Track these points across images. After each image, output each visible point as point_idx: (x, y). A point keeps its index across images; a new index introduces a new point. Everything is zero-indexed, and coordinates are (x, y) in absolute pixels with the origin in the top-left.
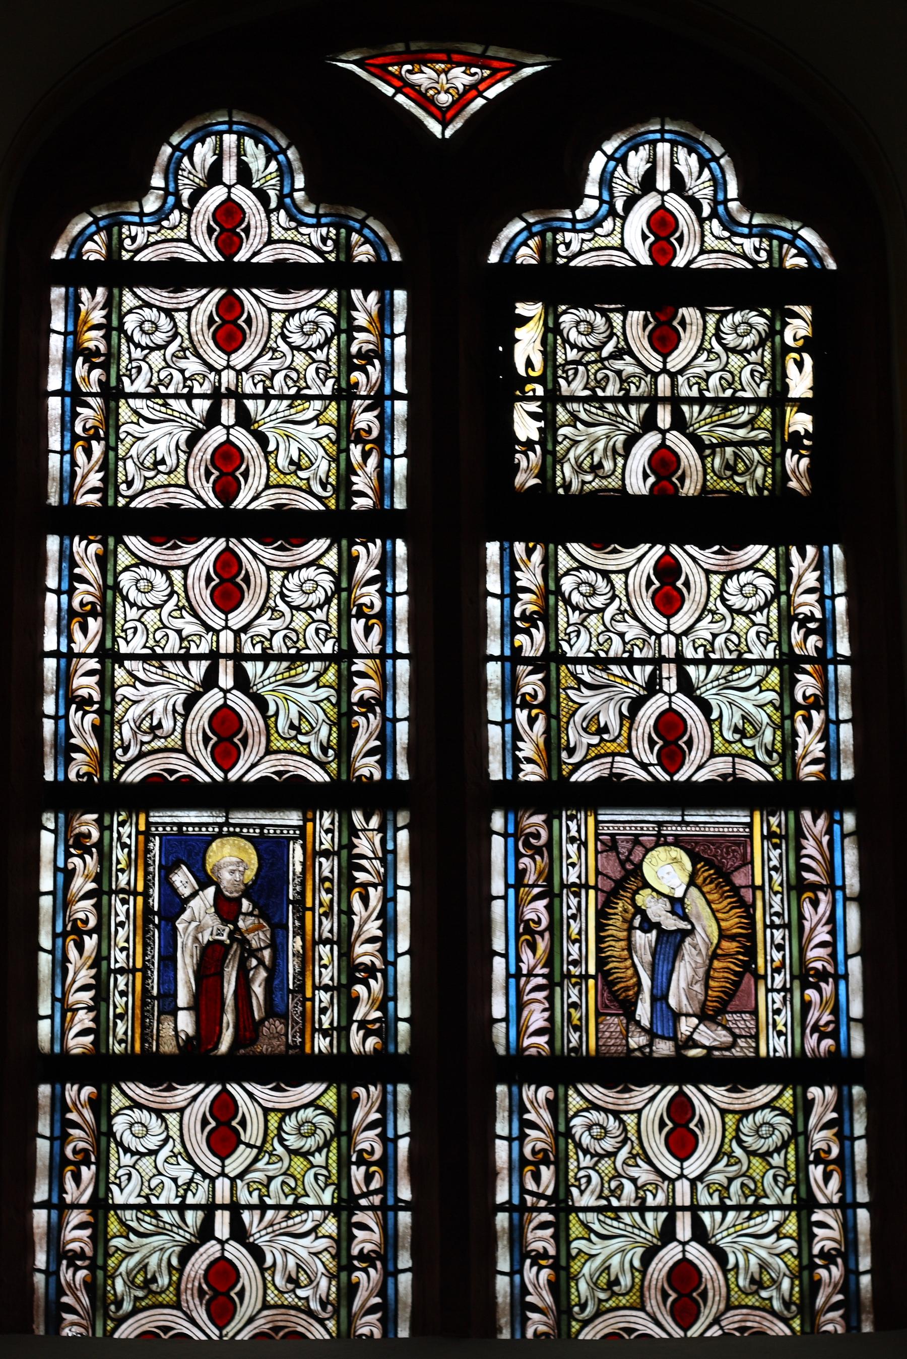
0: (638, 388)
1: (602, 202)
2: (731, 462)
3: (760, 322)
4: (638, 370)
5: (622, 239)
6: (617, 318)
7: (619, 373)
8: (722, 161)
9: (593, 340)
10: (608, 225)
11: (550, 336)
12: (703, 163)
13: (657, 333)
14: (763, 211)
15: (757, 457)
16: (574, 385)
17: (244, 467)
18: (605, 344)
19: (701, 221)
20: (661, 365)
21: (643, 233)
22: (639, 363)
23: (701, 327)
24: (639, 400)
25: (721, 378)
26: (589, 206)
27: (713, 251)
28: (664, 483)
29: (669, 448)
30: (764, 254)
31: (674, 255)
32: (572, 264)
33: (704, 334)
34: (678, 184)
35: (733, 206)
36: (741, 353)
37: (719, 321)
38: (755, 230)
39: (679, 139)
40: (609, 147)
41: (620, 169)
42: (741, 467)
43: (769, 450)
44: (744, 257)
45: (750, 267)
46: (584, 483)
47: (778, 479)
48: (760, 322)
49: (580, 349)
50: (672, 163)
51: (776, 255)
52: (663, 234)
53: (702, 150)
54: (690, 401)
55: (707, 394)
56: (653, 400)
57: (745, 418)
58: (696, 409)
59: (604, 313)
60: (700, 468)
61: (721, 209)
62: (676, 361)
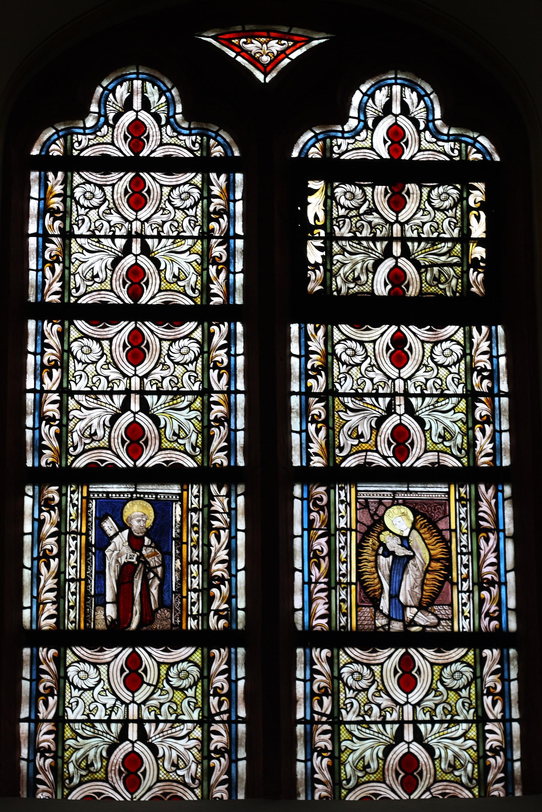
0: (381, 232)
1: (360, 121)
2: (437, 276)
3: (454, 193)
4: (381, 221)
5: (372, 143)
6: (369, 190)
7: (370, 223)
8: (432, 96)
9: (355, 203)
10: (363, 134)
11: (329, 201)
12: (420, 98)
13: (393, 199)
14: (456, 126)
15: (452, 273)
16: (343, 230)
18: (361, 205)
19: (419, 132)
20: (395, 218)
21: (384, 139)
22: (382, 217)
23: (419, 196)
24: (382, 239)
25: (431, 226)
26: (352, 123)
27: (426, 150)
28: (397, 289)
29: (400, 268)
30: (456, 152)
31: (403, 153)
32: (342, 158)
33: (421, 200)
34: (405, 110)
35: (438, 123)
36: (443, 211)
37: (430, 192)
38: (451, 138)
39: (406, 83)
40: (364, 88)
41: (370, 101)
42: (443, 279)
43: (460, 269)
44: (445, 153)
45: (448, 159)
46: (349, 288)
47: (465, 286)
48: (454, 193)
49: (346, 209)
50: (402, 97)
51: (464, 153)
52: (396, 140)
53: (420, 90)
54: (412, 240)
55: (423, 235)
56: (390, 239)
57: (445, 250)
58: (416, 244)
59: (361, 187)
60: (418, 279)
61: (431, 125)
62: (404, 216)
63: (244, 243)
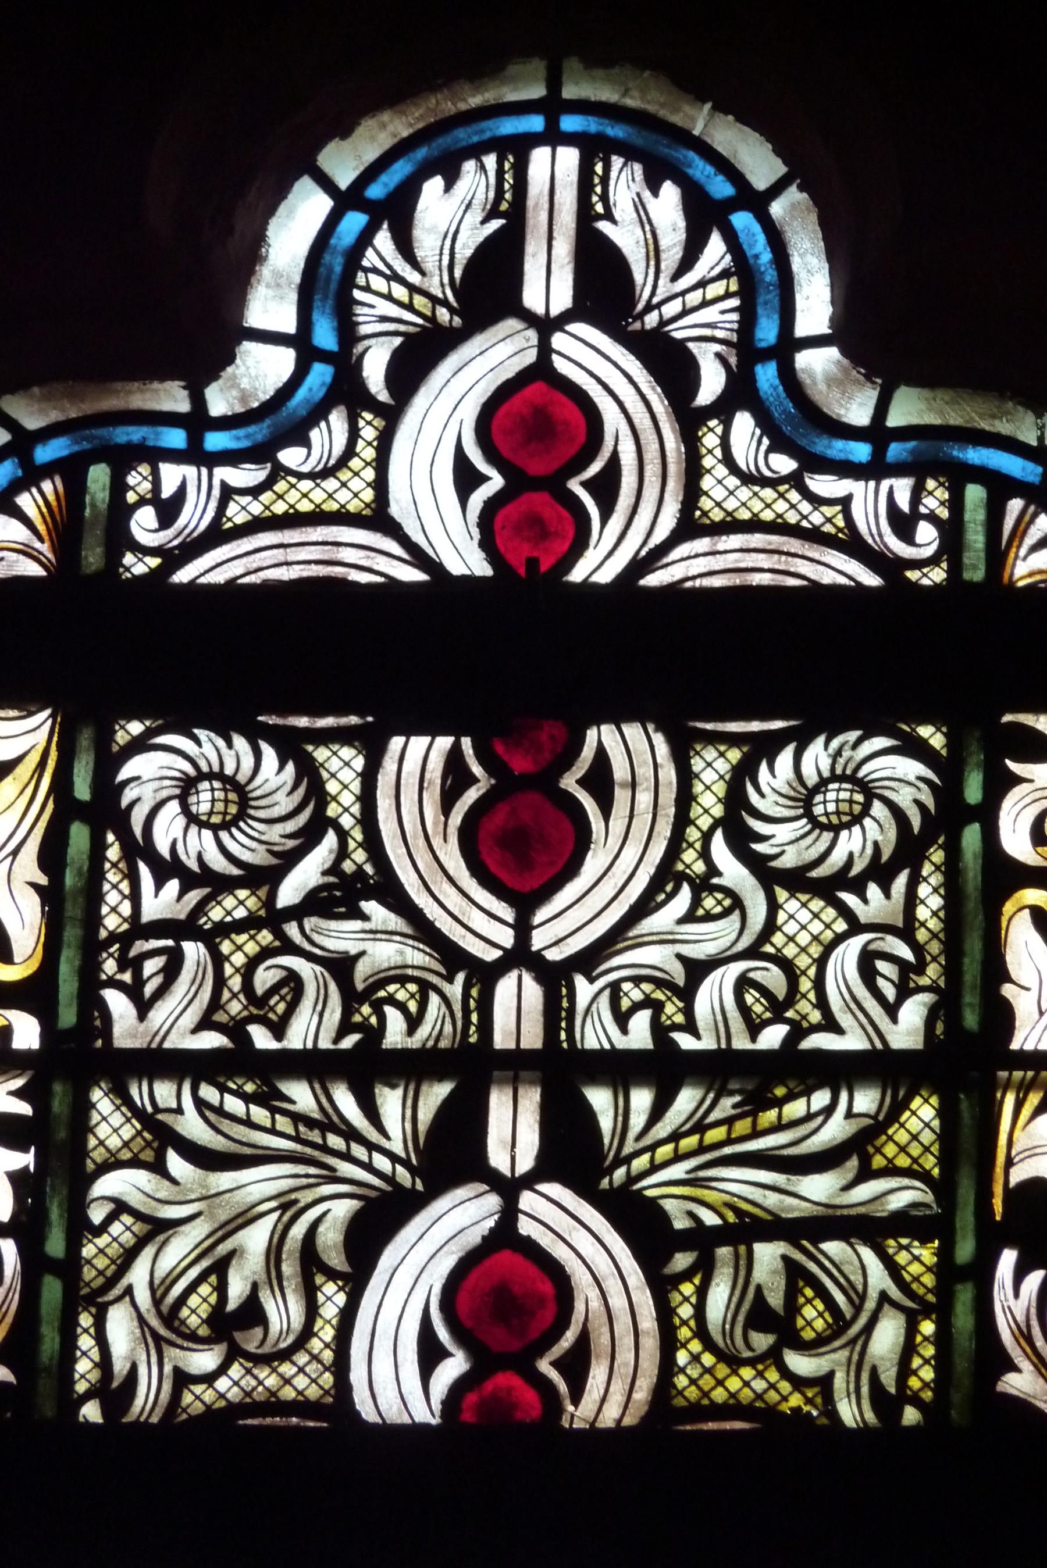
0: (413, 1023)
1: (307, 353)
2: (775, 1300)
3: (902, 776)
4: (416, 956)
5: (381, 485)
6: (341, 766)
7: (340, 967)
8: (777, 209)
9: (247, 847)
10: (331, 435)
11: (79, 835)
12: (703, 216)
13: (498, 819)
14: (928, 379)
15: (878, 1277)
16: (159, 1015)
17: (570, 1337)
18: (289, 860)
19: (690, 421)
20: (506, 938)
21: (461, 461)
22: (424, 931)
23: (669, 796)
24: (413, 1068)
25: (743, 983)
26: (261, 370)
27: (731, 526)
28: (507, 1380)
29: (531, 1249)
30: (926, 533)
31: (580, 543)
32: (183, 576)
33: (682, 820)
34: (604, 288)
35: (817, 364)
36: (827, 889)
37: (742, 776)
38: (896, 451)
39: (616, 131)
40: (343, 162)
41: (383, 240)
42: (812, 1316)
43: (927, 1254)
44: (852, 544)
45: (871, 579)
46: (182, 1379)
47: (962, 1364)
48: (902, 776)
49: (189, 881)
50: (585, 216)
51: (976, 538)
52: (537, 467)
53: (700, 169)
54: (619, 1069)
55: (685, 1042)
56: (473, 1066)
57: (835, 1130)
58: (642, 1099)
59: (292, 747)
60: (648, 1321)
61: (767, 375)
62: (566, 923)
63: (523, 1070)
